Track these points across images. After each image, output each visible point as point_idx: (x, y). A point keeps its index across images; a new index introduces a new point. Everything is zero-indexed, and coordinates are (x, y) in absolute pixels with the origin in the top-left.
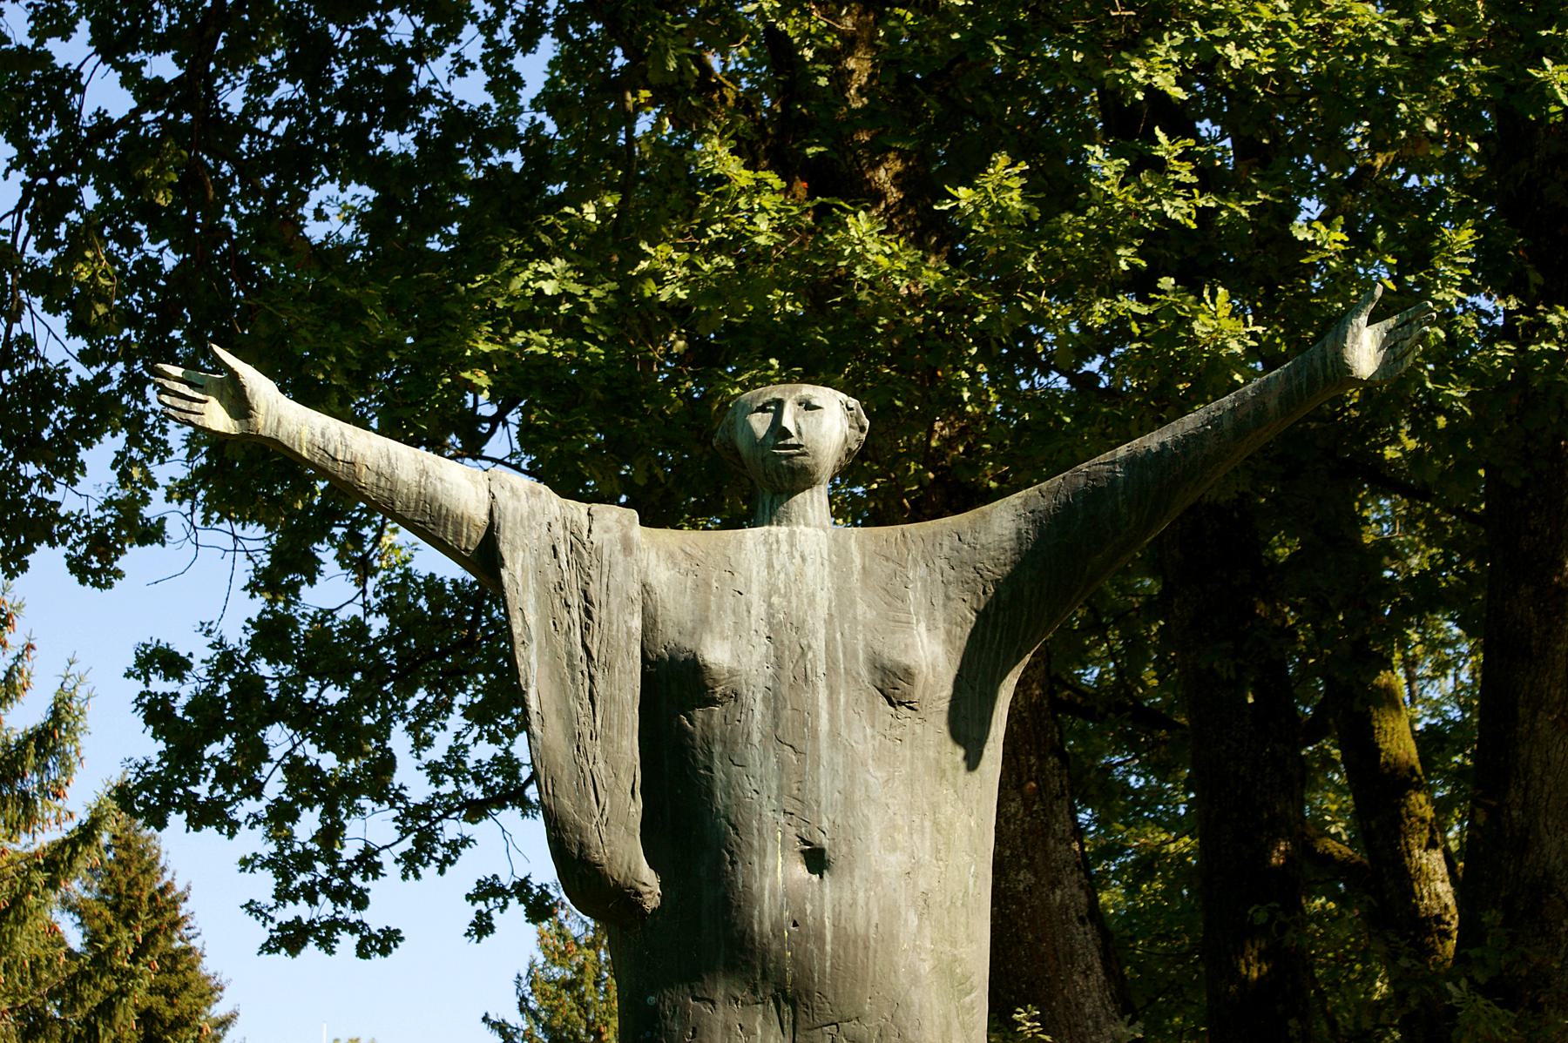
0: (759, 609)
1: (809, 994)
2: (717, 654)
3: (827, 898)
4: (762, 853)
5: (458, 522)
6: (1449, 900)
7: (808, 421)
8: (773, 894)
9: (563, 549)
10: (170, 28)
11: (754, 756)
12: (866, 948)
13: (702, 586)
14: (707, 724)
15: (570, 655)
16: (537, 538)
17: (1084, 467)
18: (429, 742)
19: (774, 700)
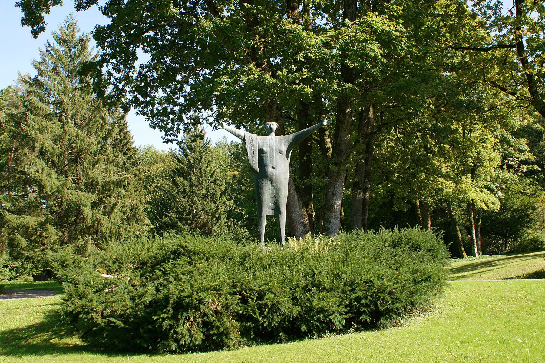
0: (268, 144)
2: (265, 149)
6: (330, 145)
11: (268, 158)
19: (270, 154)
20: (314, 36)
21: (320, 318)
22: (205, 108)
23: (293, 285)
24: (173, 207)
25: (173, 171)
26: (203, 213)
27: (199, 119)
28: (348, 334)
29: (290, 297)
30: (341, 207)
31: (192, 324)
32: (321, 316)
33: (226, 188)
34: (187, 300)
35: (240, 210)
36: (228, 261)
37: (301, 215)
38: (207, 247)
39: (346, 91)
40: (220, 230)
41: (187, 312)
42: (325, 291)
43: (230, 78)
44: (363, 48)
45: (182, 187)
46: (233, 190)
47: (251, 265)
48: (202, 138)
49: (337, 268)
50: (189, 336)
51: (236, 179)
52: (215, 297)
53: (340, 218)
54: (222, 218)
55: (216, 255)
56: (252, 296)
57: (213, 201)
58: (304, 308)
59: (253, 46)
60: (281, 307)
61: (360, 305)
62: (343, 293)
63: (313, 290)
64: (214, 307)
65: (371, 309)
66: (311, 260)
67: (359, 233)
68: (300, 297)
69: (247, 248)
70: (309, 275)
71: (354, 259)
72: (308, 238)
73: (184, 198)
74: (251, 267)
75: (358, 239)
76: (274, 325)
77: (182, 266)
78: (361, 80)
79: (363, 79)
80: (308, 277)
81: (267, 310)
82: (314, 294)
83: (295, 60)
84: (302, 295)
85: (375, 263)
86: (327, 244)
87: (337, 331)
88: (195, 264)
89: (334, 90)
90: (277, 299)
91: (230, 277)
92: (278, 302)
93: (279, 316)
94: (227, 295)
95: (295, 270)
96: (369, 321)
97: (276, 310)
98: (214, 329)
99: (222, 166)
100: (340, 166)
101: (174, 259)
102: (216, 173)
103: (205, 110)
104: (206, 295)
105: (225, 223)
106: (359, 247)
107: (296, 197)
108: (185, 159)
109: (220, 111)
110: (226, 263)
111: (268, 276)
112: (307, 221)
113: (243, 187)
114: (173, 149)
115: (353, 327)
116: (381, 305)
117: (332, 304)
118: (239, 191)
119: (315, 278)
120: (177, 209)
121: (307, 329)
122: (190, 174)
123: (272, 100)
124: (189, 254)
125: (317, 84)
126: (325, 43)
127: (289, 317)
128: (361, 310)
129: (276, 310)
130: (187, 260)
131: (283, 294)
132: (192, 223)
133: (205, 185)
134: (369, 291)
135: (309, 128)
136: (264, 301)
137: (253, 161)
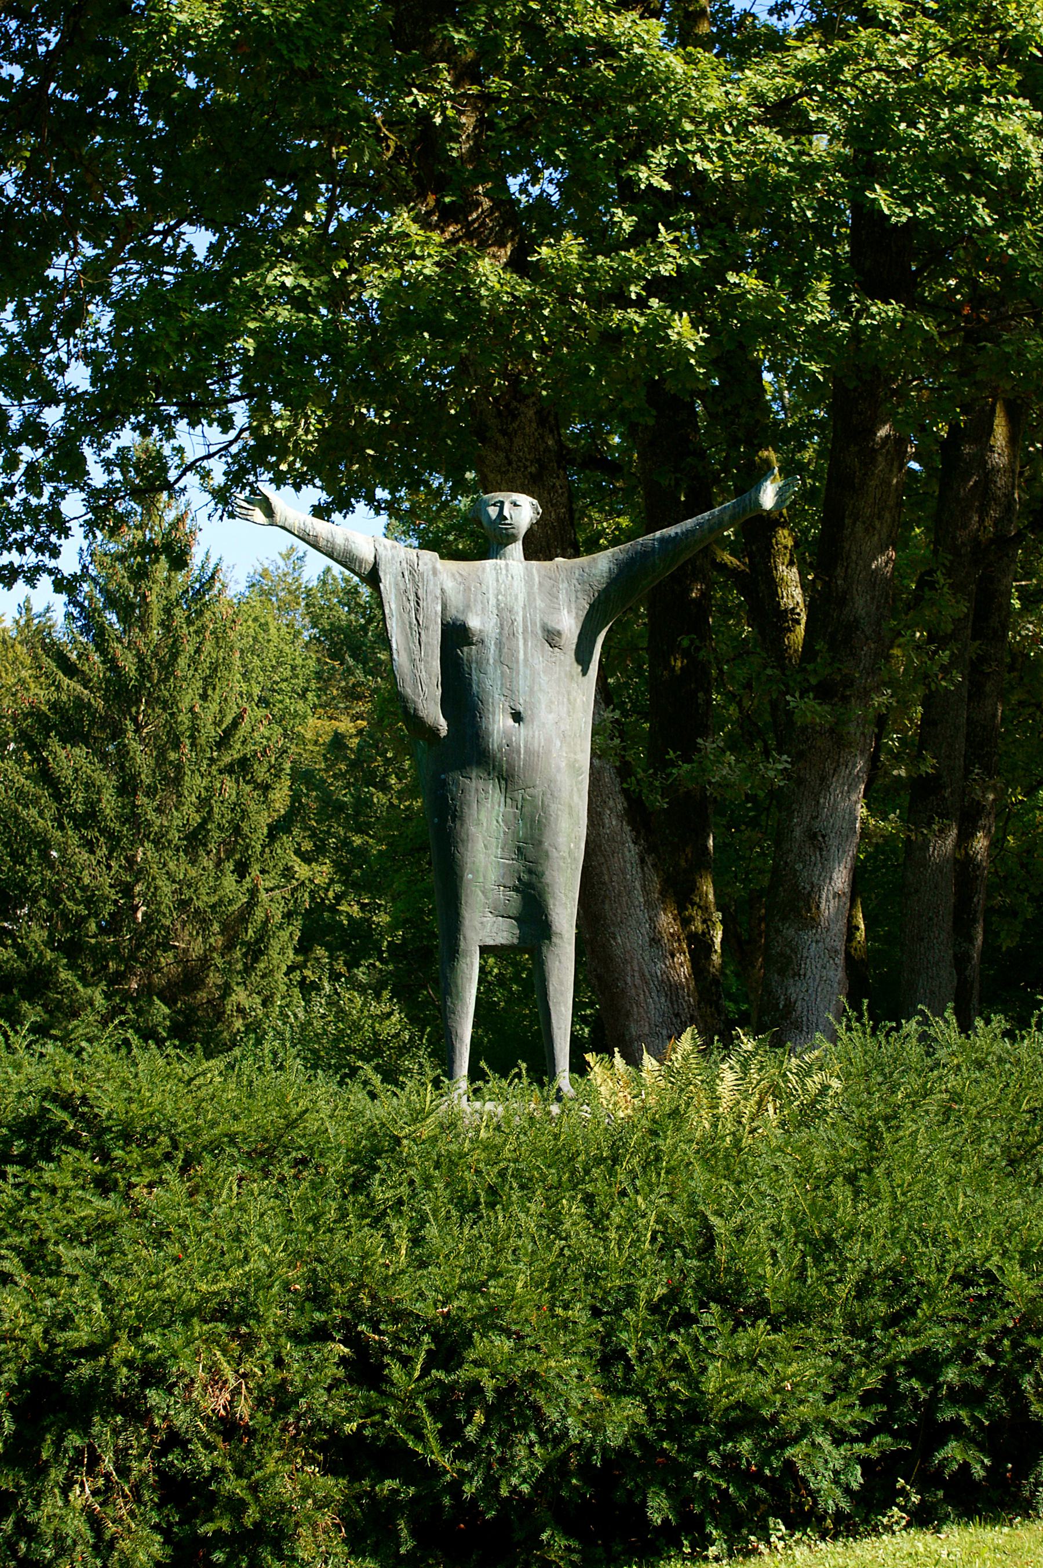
0: (493, 601)
2: (474, 622)
4: (494, 714)
6: (799, 599)
7: (515, 512)
9: (406, 573)
10: (19, 49)
11: (490, 669)
13: (467, 589)
14: (469, 654)
16: (396, 568)
17: (640, 540)
19: (500, 645)
20: (722, 70)
21: (738, 1456)
22: (194, 414)
23: (607, 1293)
24: (36, 893)
25: (34, 713)
26: (184, 924)
27: (165, 469)
28: (879, 1535)
29: (589, 1353)
30: (853, 901)
31: (109, 1487)
32: (746, 1445)
33: (296, 797)
34: (85, 1370)
35: (363, 907)
36: (289, 1172)
37: (655, 941)
38: (187, 1105)
39: (875, 336)
40: (264, 1004)
41: (85, 1428)
42: (761, 1323)
43: (309, 273)
44: (959, 130)
45: (78, 800)
46: (330, 807)
47: (404, 1190)
48: (179, 561)
49: (823, 1208)
50: (95, 1547)
51: (346, 758)
52: (224, 1352)
53: (848, 953)
54: (275, 945)
55: (232, 1142)
56: (404, 1348)
57: (230, 866)
58: (660, 1409)
59: (424, 117)
60: (549, 1400)
61: (933, 1395)
62: (852, 1330)
63: (707, 1319)
64: (216, 1402)
65: (989, 1415)
66: (697, 1168)
67: (931, 1032)
68: (641, 1352)
69: (380, 1111)
70: (686, 1243)
71: (904, 1165)
72: (685, 1058)
73: (90, 846)
74: (400, 1202)
75: (929, 1061)
76: (514, 1490)
77: (64, 1200)
78: (952, 282)
79: (956, 276)
80: (679, 1253)
81: (479, 1417)
82: (710, 1339)
83: (628, 186)
84: (650, 1342)
85: (1011, 1184)
86: (775, 1091)
87: (822, 1519)
88: (131, 1186)
89: (816, 329)
90: (528, 1360)
91: (298, 1254)
92: (532, 1377)
93: (536, 1449)
94: (283, 1340)
95: (616, 1217)
96: (978, 1472)
97: (521, 1414)
98: (216, 1511)
99: (280, 691)
100: (845, 699)
101: (25, 1161)
102: (245, 727)
103: (193, 424)
104: (177, 1342)
105: (291, 969)
106: (932, 1104)
107: (631, 851)
108: (96, 657)
109: (260, 427)
110: (282, 1180)
111: (485, 1249)
112: (685, 971)
113: (379, 798)
114: (37, 608)
115: (900, 1500)
116: (1037, 1394)
117: (795, 1385)
118: (357, 813)
119: (712, 1256)
120: (54, 900)
121: (678, 1513)
122: (118, 733)
123: (514, 379)
124: (98, 1136)
125: (734, 300)
126: (775, 105)
127: (585, 1450)
128: (939, 1417)
129: (521, 1414)
130: (88, 1166)
131: (555, 1338)
132: (130, 969)
133: (194, 784)
134: (977, 1324)
135: (689, 523)
136: (465, 1373)
137: (417, 681)
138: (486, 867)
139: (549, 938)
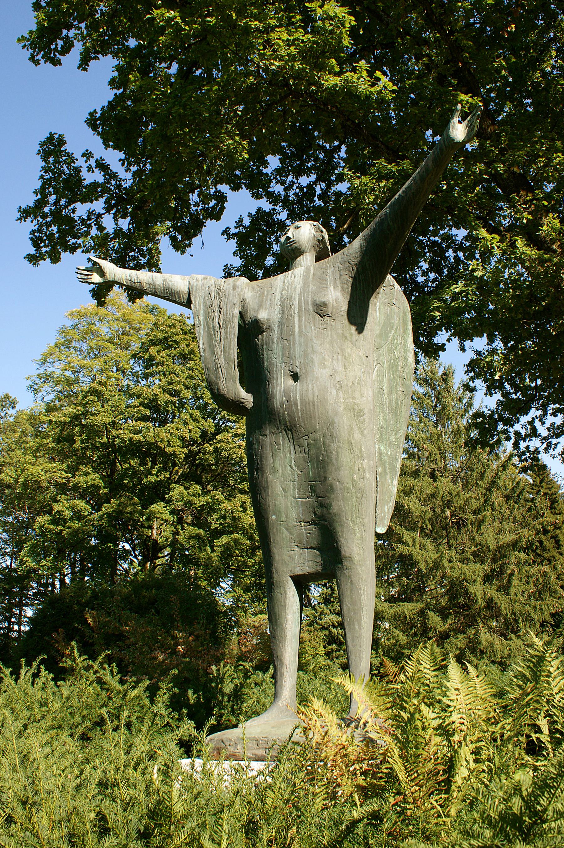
0: (278, 296)
1: (295, 426)
2: (262, 315)
3: (298, 390)
5: (179, 294)
8: (280, 392)
12: (314, 405)
14: (262, 340)
15: (214, 327)
16: (202, 293)
18: (544, 423)
19: (281, 325)
138: (287, 507)
139: (341, 562)
